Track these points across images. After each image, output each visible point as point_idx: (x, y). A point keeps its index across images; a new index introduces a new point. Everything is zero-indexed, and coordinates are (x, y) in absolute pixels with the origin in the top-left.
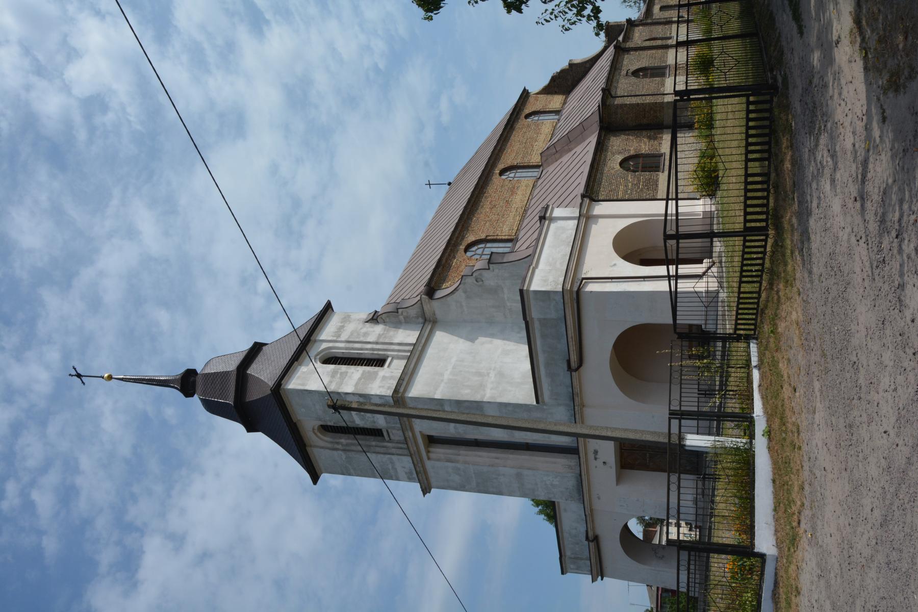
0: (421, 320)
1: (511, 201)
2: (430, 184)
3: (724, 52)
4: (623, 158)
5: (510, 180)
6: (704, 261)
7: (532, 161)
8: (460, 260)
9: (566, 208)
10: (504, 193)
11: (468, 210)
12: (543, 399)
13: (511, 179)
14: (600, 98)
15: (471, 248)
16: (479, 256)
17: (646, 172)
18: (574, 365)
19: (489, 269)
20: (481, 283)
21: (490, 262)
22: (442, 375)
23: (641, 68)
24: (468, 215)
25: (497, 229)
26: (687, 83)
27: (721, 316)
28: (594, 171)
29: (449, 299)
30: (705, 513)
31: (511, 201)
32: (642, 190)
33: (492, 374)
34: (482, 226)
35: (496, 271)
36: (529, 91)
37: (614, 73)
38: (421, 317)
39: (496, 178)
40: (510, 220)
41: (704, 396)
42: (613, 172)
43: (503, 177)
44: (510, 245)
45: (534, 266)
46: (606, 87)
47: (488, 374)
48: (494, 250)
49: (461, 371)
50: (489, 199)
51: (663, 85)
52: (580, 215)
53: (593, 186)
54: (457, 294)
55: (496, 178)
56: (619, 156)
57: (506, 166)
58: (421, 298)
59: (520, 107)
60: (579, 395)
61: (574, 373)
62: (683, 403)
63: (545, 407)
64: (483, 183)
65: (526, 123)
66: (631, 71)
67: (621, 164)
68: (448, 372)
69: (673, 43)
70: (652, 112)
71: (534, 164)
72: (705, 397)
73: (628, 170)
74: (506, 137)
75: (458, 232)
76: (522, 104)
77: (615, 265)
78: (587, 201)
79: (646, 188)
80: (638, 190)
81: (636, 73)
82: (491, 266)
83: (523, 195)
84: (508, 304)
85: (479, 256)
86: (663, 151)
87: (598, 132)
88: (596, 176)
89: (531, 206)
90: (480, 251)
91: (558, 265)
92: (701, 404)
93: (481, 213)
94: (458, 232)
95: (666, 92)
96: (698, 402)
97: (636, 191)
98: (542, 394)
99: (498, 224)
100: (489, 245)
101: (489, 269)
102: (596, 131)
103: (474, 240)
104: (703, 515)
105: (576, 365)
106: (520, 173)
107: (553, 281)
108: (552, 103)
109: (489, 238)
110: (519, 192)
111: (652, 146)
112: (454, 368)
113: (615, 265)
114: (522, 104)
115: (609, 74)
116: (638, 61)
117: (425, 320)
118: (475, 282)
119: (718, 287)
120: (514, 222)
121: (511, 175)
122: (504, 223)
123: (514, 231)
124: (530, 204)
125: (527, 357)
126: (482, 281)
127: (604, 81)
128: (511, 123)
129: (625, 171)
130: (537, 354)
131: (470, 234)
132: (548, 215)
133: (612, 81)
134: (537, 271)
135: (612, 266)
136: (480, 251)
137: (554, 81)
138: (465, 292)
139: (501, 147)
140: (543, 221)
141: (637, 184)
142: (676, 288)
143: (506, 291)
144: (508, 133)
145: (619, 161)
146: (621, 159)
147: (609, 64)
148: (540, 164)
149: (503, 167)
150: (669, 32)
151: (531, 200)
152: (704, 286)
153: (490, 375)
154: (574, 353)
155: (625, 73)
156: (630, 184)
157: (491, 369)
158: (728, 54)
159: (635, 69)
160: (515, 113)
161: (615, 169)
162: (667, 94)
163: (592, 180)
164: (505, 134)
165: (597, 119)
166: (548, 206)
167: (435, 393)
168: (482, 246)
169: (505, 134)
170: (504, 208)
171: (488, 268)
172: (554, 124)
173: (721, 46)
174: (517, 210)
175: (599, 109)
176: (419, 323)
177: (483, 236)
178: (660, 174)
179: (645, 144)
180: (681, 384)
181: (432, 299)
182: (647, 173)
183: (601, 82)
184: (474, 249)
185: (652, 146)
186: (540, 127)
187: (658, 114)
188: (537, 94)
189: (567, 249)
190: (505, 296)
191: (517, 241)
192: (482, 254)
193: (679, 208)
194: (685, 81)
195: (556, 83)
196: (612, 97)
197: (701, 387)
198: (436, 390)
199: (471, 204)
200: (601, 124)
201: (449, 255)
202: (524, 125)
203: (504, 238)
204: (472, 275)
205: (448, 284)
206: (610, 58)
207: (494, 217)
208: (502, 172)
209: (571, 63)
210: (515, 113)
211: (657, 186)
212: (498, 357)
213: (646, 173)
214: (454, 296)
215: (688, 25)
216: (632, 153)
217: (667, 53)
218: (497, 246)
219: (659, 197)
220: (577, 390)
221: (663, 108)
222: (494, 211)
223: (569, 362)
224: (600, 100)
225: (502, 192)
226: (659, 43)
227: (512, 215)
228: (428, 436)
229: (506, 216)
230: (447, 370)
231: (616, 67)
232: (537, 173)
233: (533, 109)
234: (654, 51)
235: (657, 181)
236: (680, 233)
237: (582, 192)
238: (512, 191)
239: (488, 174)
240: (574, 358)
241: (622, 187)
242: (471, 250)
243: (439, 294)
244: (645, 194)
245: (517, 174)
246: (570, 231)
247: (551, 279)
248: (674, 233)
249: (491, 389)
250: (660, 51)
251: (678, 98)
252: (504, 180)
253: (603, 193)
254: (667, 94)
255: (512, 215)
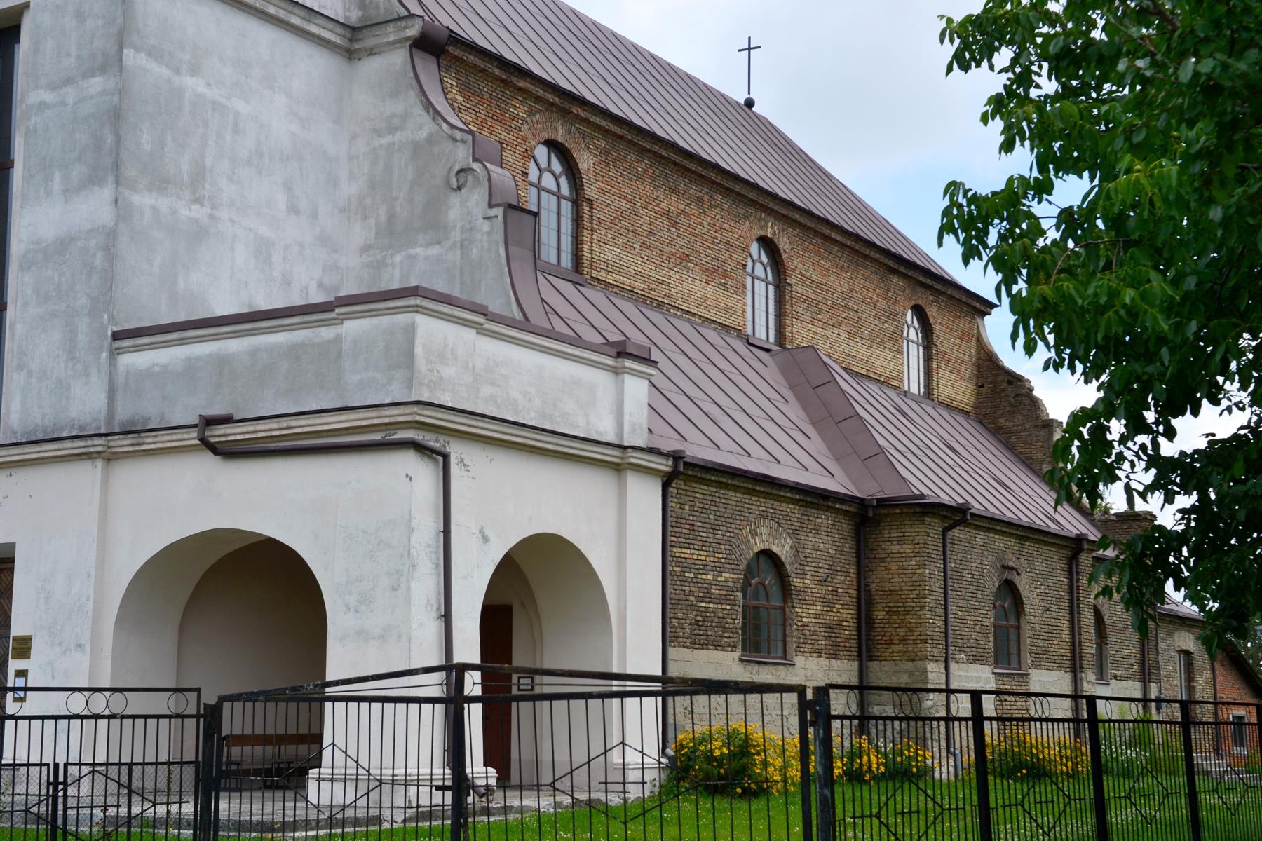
0: (354, 16)
1: (687, 268)
2: (749, 49)
3: (1069, 803)
4: (783, 559)
5: (744, 266)
6: (490, 769)
7: (797, 325)
8: (525, 128)
9: (646, 409)
10: (710, 248)
11: (664, 153)
12: (128, 350)
13: (749, 269)
14: (945, 499)
15: (556, 155)
16: (535, 180)
17: (744, 617)
18: (218, 434)
19: (491, 206)
20: (455, 184)
21: (514, 208)
22: (195, 71)
23: (1022, 603)
24: (650, 151)
25: (610, 229)
26: (1110, 721)
27: (315, 817)
28: (746, 485)
29: (413, 95)
30: (403, 782)
31: (687, 268)
32: (693, 607)
33: (198, 212)
34: (619, 188)
35: (486, 226)
36: (986, 318)
37: (1010, 535)
38: (363, 16)
39: (751, 229)
40: (635, 264)
41: (51, 780)
42: (746, 532)
43: (754, 248)
44: (567, 262)
45: (486, 326)
46: (973, 515)
47: (198, 201)
48: (548, 220)
49: (206, 124)
50: (693, 210)
51: (973, 660)
52: (626, 448)
53: (708, 483)
54: (426, 119)
55: (751, 229)
56: (787, 547)
57: (784, 256)
58: (414, 15)
59: (944, 293)
60: (137, 448)
61: (194, 434)
62: (23, 724)
63: (104, 355)
64: (739, 194)
65: (899, 309)
66: (1016, 579)
67: (767, 554)
68: (202, 89)
69: (1085, 685)
70: (902, 632)
71: (788, 329)
72: (49, 784)
73: (749, 573)
74: (865, 257)
75: (603, 123)
76: (951, 297)
77: (486, 539)
78: (665, 465)
79: (699, 618)
80: (692, 598)
81: (1009, 589)
82: (499, 211)
83: (704, 299)
84: (398, 258)
85: (535, 180)
86: (799, 660)
87: (857, 494)
88: (736, 488)
89: (671, 319)
90: (548, 181)
91: (486, 391)
92: (34, 771)
93: (656, 187)
94: (603, 123)
95: (953, 666)
96: (156, 764)
97: (691, 593)
98: (139, 349)
99: (623, 232)
100: (566, 207)
101: (491, 206)
102: (859, 491)
103: (580, 166)
104: (487, 777)
105: (217, 439)
106: (763, 293)
107: (441, 378)
108: (953, 376)
109: (586, 208)
110: (710, 290)
111: (814, 633)
112: (216, 105)
113: (486, 539)
114: (951, 297)
115: (1009, 524)
116: (1042, 596)
117: (353, 31)
118: (457, 168)
119: (418, 806)
120: (628, 277)
121: (759, 267)
122: (628, 247)
123: (602, 275)
124: (678, 317)
125: (250, 306)
126: (459, 188)
127: (993, 510)
128: (903, 269)
129: (746, 563)
130: (247, 333)
131: (596, 156)
132: (629, 363)
133: (989, 530)
134: (470, 334)
135: (481, 531)
136: (548, 181)
137: (1010, 383)
138: (430, 140)
139: (836, 241)
140: (613, 351)
141: (708, 595)
142: (334, 699)
143: (434, 251)
144: (877, 261)
145: (775, 549)
146: (779, 553)
147: (1038, 522)
148: (788, 346)
149: (781, 246)
150: (1119, 673)
151: (690, 321)
152: (421, 771)
153: (195, 207)
154: (248, 433)
155: (1011, 564)
156: (710, 577)
157: (213, 207)
158: (934, 823)
159: (1020, 588)
160: (928, 281)
161: (754, 538)
162: (947, 668)
163: (725, 480)
164: (873, 254)
165: (889, 493)
166: (654, 363)
167: (138, 49)
168: (565, 190)
169: (873, 254)
170: (667, 249)
171: (493, 203)
172: (894, 383)
173: (1038, 806)
174: (662, 282)
175: (915, 497)
176: (347, 9)
177: (590, 192)
178: (737, 655)
179: (817, 616)
180: (109, 717)
181: (410, 46)
182: (739, 622)
183: (985, 501)
184: (557, 167)
185: (814, 633)
186: (887, 345)
187: (896, 648)
188: (979, 339)
189: (533, 414)
190: (419, 250)
191: (574, 283)
192: (539, 188)
193: (565, 702)
194: (1114, 718)
195: (1005, 385)
196: (945, 531)
197: (137, 770)
198: (149, 54)
199: (679, 159)
200: (875, 503)
201: (538, 99)
202: (896, 302)
203: (586, 247)
204: (475, 159)
205: (455, 94)
206: (1052, 525)
207: (643, 222)
208: (768, 244)
209: (1055, 425)
210: (928, 281)
211: (703, 646)
212: (250, 229)
213: (740, 617)
214: (418, 110)
215: (1068, 720)
216: (796, 582)
217: (1060, 668)
218: (563, 229)
219: (672, 651)
220: (150, 442)
221: (913, 660)
222: (662, 222)
223: (228, 420)
224: (938, 501)
225: (713, 243)
226: (1090, 649)
227: (649, 269)
228: (20, 25)
229: (645, 253)
230: (208, 84)
231: (1027, 539)
232: (764, 337)
233: (937, 328)
234: (1066, 635)
235: (718, 646)
236: (466, 706)
237: (688, 453)
238: (715, 271)
239: (762, 206)
240: (235, 433)
241: (701, 555)
242: (553, 156)
243: (428, 68)
244: (680, 615)
245: (763, 284)
246: (582, 422)
247: (448, 371)
248: (466, 693)
249: (155, 209)
250: (1066, 651)
251: (809, 696)
252: (746, 249)
253: (687, 507)
254: (947, 668)
255: (649, 269)
